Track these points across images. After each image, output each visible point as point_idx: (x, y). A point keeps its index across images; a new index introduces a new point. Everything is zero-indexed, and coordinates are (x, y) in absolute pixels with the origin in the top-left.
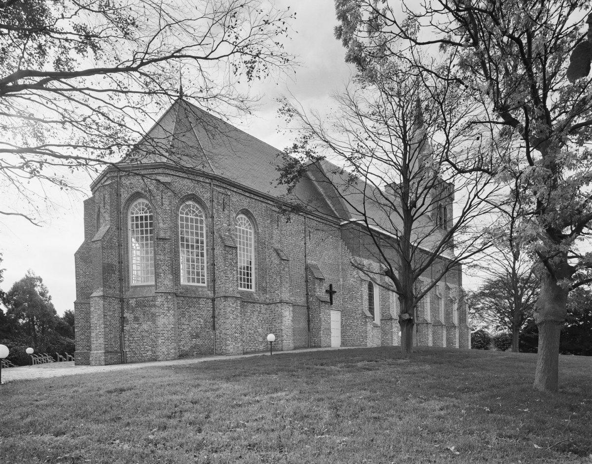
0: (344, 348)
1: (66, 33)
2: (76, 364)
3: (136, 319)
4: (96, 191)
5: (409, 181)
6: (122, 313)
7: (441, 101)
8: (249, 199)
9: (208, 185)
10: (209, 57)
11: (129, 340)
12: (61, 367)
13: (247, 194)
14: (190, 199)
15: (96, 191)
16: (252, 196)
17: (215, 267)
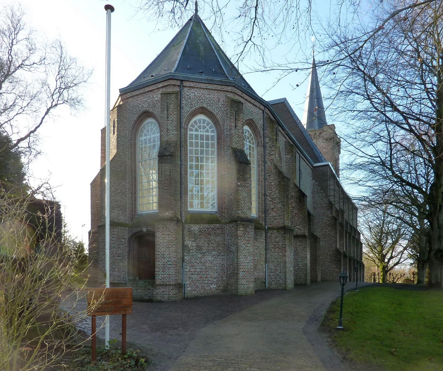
3: (199, 248)
11: (190, 271)
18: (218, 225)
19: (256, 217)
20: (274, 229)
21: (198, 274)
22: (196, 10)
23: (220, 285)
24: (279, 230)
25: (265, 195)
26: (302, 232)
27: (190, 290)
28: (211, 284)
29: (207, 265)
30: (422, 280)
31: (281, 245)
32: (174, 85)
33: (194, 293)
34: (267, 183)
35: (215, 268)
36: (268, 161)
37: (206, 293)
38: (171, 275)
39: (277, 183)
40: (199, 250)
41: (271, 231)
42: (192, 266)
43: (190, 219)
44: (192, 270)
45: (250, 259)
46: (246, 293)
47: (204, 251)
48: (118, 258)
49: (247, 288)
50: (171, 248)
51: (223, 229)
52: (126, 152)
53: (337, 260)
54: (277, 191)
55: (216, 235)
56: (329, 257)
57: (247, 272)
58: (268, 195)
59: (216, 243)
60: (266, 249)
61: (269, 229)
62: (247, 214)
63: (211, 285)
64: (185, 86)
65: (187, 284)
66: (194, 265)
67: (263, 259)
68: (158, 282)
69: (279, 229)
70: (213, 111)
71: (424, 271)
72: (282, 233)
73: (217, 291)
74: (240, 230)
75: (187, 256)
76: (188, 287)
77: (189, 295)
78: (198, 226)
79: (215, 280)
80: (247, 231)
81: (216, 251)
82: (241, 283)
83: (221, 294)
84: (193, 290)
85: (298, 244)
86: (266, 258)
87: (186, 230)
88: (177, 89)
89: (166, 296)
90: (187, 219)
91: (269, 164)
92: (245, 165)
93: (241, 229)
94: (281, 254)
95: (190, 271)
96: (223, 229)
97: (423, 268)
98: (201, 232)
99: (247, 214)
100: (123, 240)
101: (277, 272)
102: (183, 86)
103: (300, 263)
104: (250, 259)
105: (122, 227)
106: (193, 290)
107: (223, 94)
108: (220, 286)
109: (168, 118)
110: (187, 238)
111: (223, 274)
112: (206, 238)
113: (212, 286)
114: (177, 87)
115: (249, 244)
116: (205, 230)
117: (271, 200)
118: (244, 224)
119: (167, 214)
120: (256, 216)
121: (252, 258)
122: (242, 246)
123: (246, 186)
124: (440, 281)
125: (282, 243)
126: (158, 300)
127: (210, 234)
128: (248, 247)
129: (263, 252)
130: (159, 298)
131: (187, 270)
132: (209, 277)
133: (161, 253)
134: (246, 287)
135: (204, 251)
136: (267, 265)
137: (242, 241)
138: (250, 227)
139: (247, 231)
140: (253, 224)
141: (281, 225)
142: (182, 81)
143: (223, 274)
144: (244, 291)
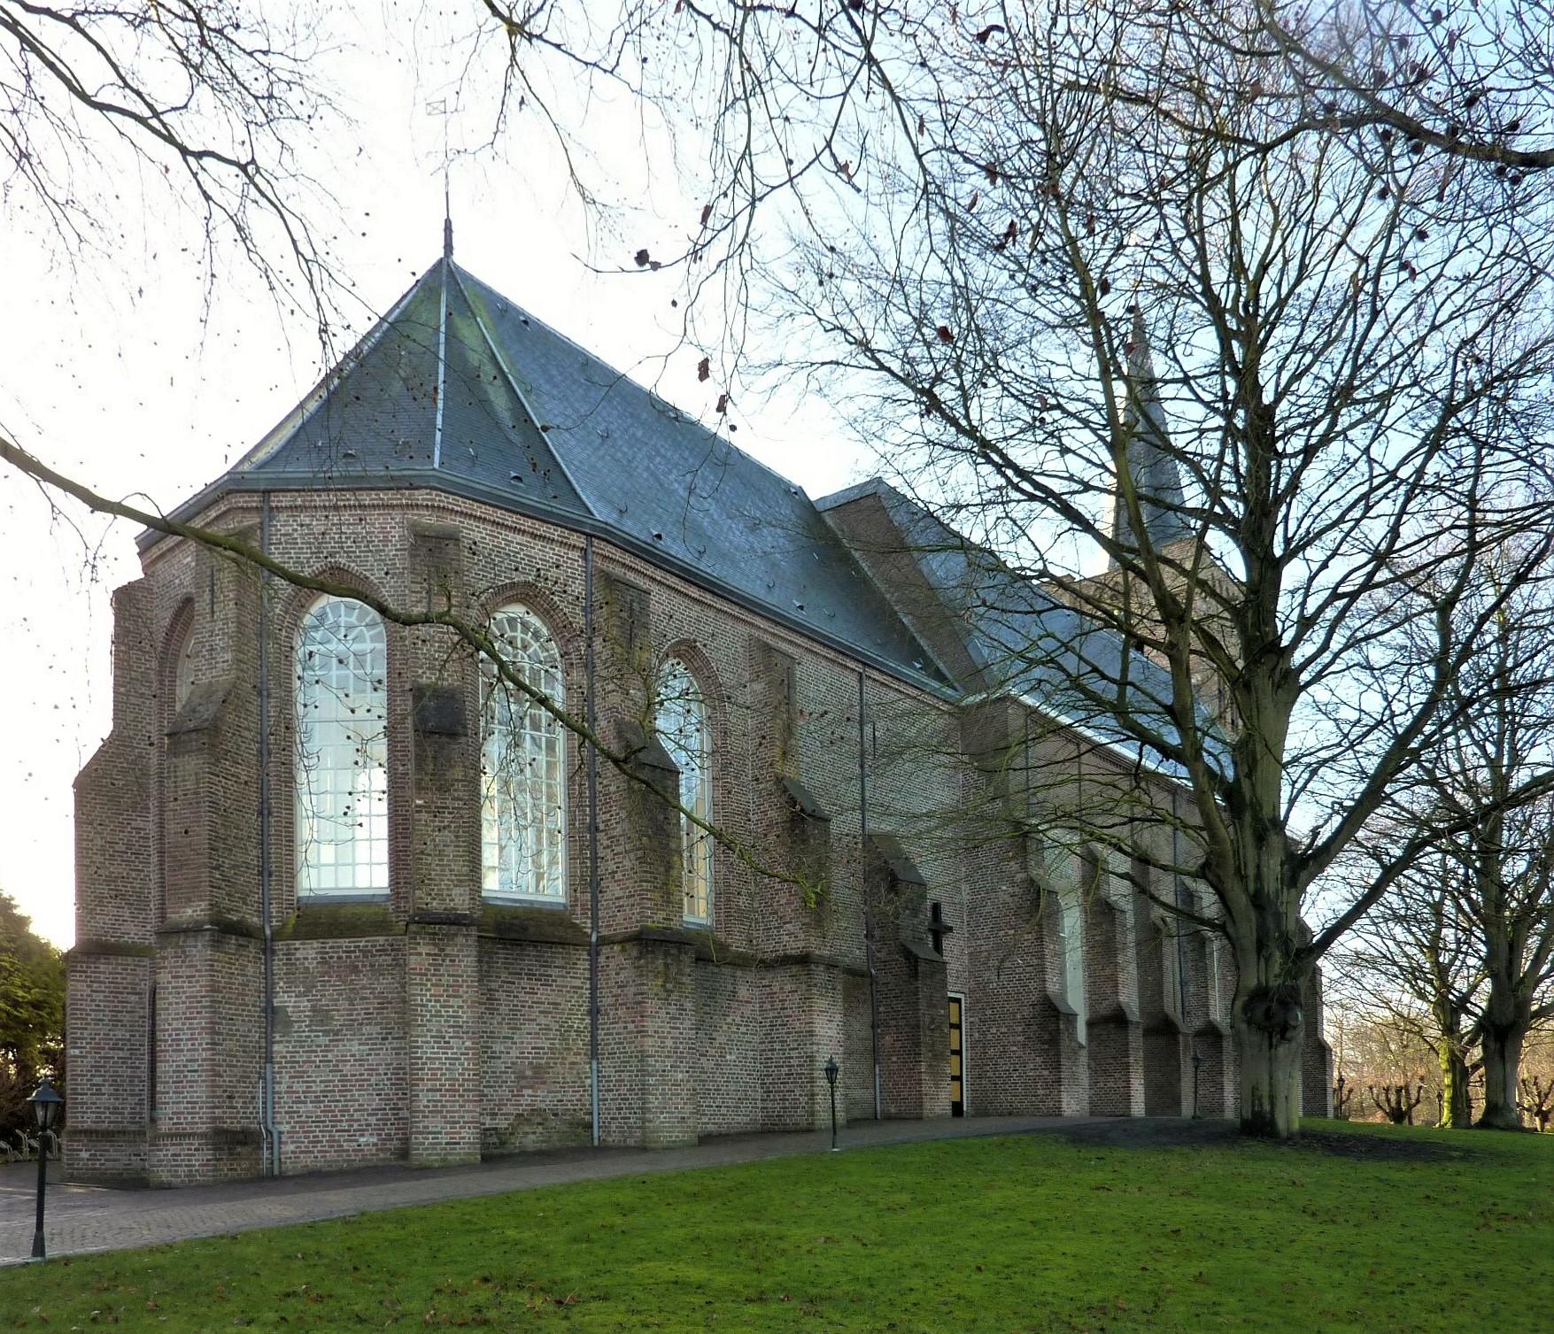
0: (1097, 1119)
1: (1399, 317)
2: (525, 929)
3: (320, 1016)
4: (154, 562)
5: (1277, 565)
6: (269, 992)
7: (1080, 182)
8: (698, 608)
9: (575, 555)
10: (1437, 323)
11: (290, 1091)
12: (551, 903)
13: (694, 592)
14: (510, 600)
15: (154, 562)
16: (708, 598)
17: (600, 836)
18: (381, 939)
19: (564, 905)
20: (614, 943)
21: (317, 1101)
22: (448, 247)
23: (389, 1135)
24: (628, 946)
25: (594, 828)
26: (801, 944)
27: (293, 1152)
28: (362, 1132)
29: (347, 1069)
30: (1501, 1102)
31: (631, 996)
32: (242, 508)
33: (307, 1161)
34: (599, 788)
35: (373, 1079)
36: (600, 715)
37: (345, 1161)
38: (196, 1103)
39: (623, 786)
40: (322, 1022)
41: (605, 950)
42: (299, 1076)
43: (297, 925)
44: (299, 1087)
45: (459, 1048)
46: (444, 1160)
47: (336, 1025)
48: (112, 1053)
49: (447, 1144)
50: (195, 1018)
51: (399, 950)
52: (148, 727)
53: (1046, 1037)
54: (623, 814)
55: (377, 971)
56: (1020, 1029)
57: (447, 1090)
58: (602, 827)
59: (375, 998)
60: (594, 1012)
61: (603, 941)
62: (452, 900)
63: (362, 1135)
64: (277, 507)
65: (280, 1133)
66: (304, 1072)
67: (581, 1044)
68: (164, 1126)
69: (626, 940)
70: (368, 574)
71: (1508, 1066)
72: (635, 953)
73: (382, 1155)
74: (420, 954)
75: (281, 1042)
76: (286, 1143)
77: (290, 1166)
78: (315, 945)
79: (373, 1120)
80: (446, 955)
81: (376, 1024)
82: (425, 1127)
83: (394, 1163)
84: (301, 1152)
85: (788, 987)
86: (594, 1044)
87: (280, 960)
88: (253, 520)
89: (182, 1171)
90: (284, 926)
91: (603, 723)
92: (445, 739)
93: (423, 950)
94: (631, 1026)
95: (290, 1091)
96: (399, 950)
97: (1503, 1058)
98: (326, 963)
99: (452, 900)
100: (133, 998)
101: (623, 1090)
102: (271, 509)
103: (794, 1054)
104: (459, 1048)
105: (130, 959)
106: (301, 1152)
107: (398, 515)
108: (389, 1138)
109: (213, 612)
110: (281, 984)
111: (399, 1099)
112: (344, 982)
113: (362, 1140)
114: (254, 514)
115: (455, 996)
116: (340, 958)
117: (609, 842)
118: (435, 934)
119: (190, 911)
120: (563, 900)
121: (468, 1044)
122: (426, 1006)
123: (447, 808)
124: (1267, 1107)
125: (633, 990)
126: (162, 1182)
127: (355, 969)
128: (452, 1007)
129: (581, 1022)
130: (165, 1177)
131: (283, 1088)
132: (355, 1111)
133: (170, 1035)
134: (444, 1139)
135: (336, 1025)
136: (594, 1066)
137: (429, 990)
138: (460, 940)
139: (446, 955)
140: (474, 932)
141: (634, 928)
142: (267, 492)
143: (399, 1099)
144: (439, 1154)
